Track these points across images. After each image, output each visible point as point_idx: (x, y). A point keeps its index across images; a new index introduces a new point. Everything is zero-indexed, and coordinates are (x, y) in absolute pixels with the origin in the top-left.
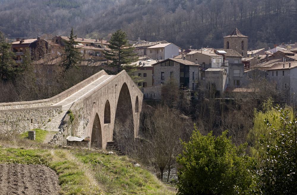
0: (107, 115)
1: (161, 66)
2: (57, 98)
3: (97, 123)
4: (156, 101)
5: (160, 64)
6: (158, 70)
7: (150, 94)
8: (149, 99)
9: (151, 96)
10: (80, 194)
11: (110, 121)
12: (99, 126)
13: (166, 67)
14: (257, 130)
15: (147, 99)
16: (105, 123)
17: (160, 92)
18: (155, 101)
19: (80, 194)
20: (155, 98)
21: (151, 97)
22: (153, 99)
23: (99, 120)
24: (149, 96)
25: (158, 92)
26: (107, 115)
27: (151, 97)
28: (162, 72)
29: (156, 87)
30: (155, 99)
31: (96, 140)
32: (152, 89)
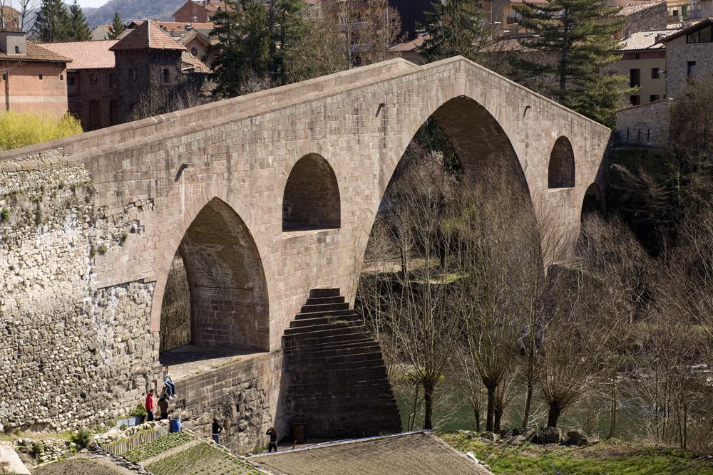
0: (330, 203)
1: (687, 43)
2: (48, 149)
3: (239, 230)
4: (649, 150)
5: (683, 38)
6: (678, 56)
7: (635, 129)
8: (631, 145)
9: (639, 136)
10: (433, 474)
11: (339, 221)
12: (247, 239)
13: (702, 45)
14: (70, 232)
15: (627, 144)
16: (286, 228)
17: (666, 124)
18: (646, 151)
19: (433, 474)
20: (650, 144)
21: (639, 139)
22: (644, 146)
23: (242, 223)
24: (634, 135)
25: (658, 122)
26: (330, 200)
27: (639, 139)
28: (690, 60)
29: (652, 108)
30: (650, 146)
31: (250, 285)
32: (642, 113)
